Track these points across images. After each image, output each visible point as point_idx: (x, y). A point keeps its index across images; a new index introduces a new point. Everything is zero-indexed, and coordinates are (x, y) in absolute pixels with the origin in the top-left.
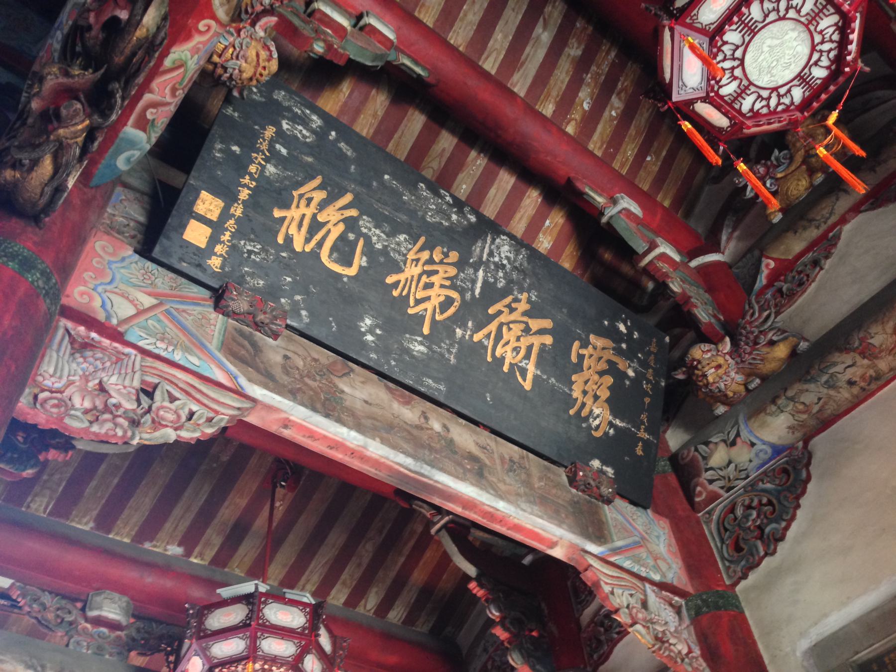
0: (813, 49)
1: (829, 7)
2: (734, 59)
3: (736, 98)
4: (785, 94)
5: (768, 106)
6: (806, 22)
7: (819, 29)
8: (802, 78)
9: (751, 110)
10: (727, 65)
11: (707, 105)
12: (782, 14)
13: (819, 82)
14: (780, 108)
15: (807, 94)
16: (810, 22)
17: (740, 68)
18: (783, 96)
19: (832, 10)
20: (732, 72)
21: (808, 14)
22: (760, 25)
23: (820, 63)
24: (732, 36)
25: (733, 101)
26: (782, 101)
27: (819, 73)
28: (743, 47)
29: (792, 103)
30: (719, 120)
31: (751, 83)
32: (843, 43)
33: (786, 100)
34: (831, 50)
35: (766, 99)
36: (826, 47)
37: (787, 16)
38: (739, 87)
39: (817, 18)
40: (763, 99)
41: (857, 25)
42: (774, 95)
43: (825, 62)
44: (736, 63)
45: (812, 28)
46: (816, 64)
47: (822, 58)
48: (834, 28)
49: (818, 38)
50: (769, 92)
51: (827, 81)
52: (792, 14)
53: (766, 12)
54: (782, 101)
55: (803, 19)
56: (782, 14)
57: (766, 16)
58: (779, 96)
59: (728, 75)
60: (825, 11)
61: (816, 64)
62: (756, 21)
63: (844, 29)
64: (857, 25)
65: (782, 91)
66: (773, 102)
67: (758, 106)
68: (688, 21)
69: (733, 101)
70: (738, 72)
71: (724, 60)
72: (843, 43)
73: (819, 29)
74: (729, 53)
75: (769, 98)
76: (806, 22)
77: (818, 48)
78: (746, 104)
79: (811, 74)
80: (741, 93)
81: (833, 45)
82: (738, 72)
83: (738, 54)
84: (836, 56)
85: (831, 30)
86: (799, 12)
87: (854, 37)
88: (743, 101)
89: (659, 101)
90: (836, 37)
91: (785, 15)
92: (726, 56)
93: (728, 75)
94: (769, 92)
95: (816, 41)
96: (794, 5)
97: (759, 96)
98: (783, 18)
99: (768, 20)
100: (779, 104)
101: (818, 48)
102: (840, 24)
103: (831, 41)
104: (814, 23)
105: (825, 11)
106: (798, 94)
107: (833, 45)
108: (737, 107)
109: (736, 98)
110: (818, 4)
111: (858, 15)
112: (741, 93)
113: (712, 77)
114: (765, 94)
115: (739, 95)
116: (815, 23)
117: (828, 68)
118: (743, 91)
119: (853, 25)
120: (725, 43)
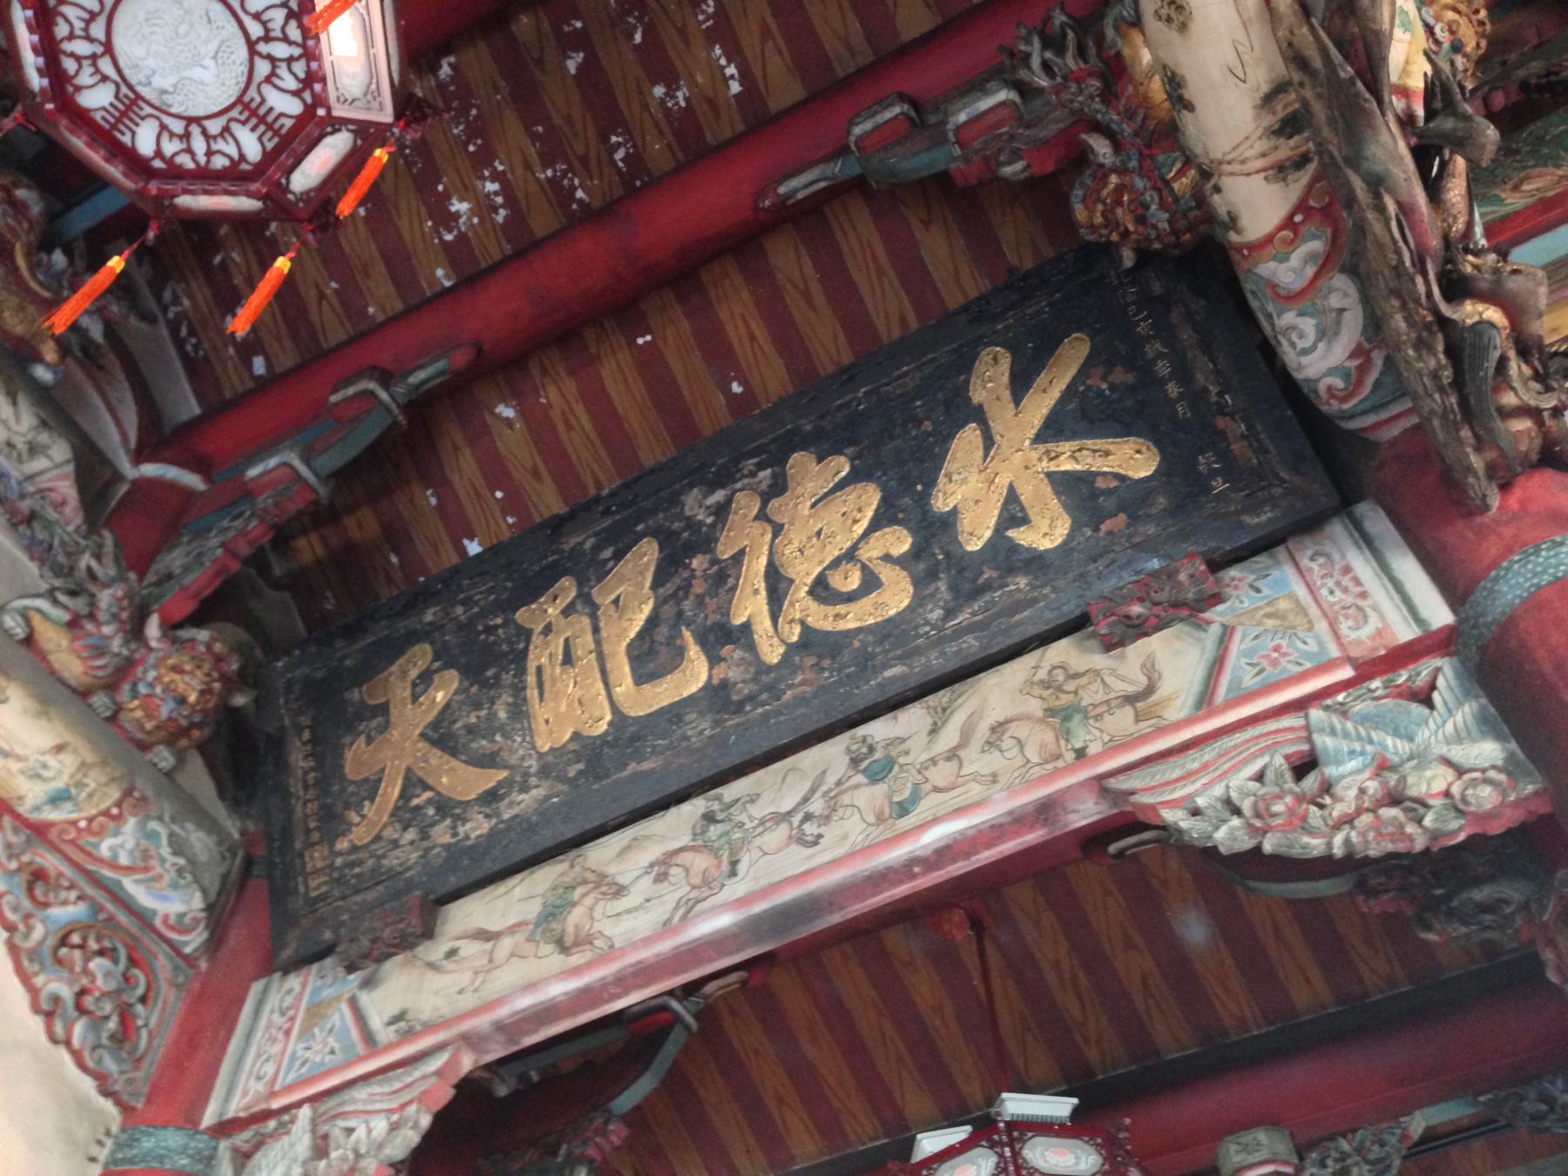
1: (276, 140)
6: (246, 99)
8: (131, 104)
9: (296, 94)
10: (199, 145)
12: (262, 48)
15: (98, 116)
16: (246, 106)
17: (206, 123)
18: (267, 30)
19: (270, 146)
20: (215, 137)
22: (124, 90)
23: (165, 137)
27: (145, 140)
28: (167, 120)
29: (78, 89)
31: (239, 100)
32: (205, 177)
33: (85, 78)
35: (274, 67)
38: (244, 123)
39: (254, 121)
40: (273, 74)
44: (195, 130)
45: (234, 113)
48: (236, 156)
50: (102, 37)
53: (265, 17)
54: (278, 34)
55: (252, 93)
56: (262, 48)
57: (105, 78)
58: (267, 38)
59: (220, 145)
60: (269, 134)
62: (117, 97)
63: (235, 176)
65: (256, 30)
67: (291, 84)
70: (214, 127)
71: (189, 151)
73: (235, 127)
75: (272, 59)
76: (246, 99)
79: (143, 118)
84: (180, 167)
90: (219, 162)
91: (260, 55)
93: (220, 145)
94: (257, 60)
97: (268, 80)
102: (244, 167)
103: (209, 153)
105: (269, 134)
106: (97, 98)
107: (202, 160)
109: (270, 127)
114: (263, 68)
116: (243, 118)
117: (159, 153)
120: (159, 153)
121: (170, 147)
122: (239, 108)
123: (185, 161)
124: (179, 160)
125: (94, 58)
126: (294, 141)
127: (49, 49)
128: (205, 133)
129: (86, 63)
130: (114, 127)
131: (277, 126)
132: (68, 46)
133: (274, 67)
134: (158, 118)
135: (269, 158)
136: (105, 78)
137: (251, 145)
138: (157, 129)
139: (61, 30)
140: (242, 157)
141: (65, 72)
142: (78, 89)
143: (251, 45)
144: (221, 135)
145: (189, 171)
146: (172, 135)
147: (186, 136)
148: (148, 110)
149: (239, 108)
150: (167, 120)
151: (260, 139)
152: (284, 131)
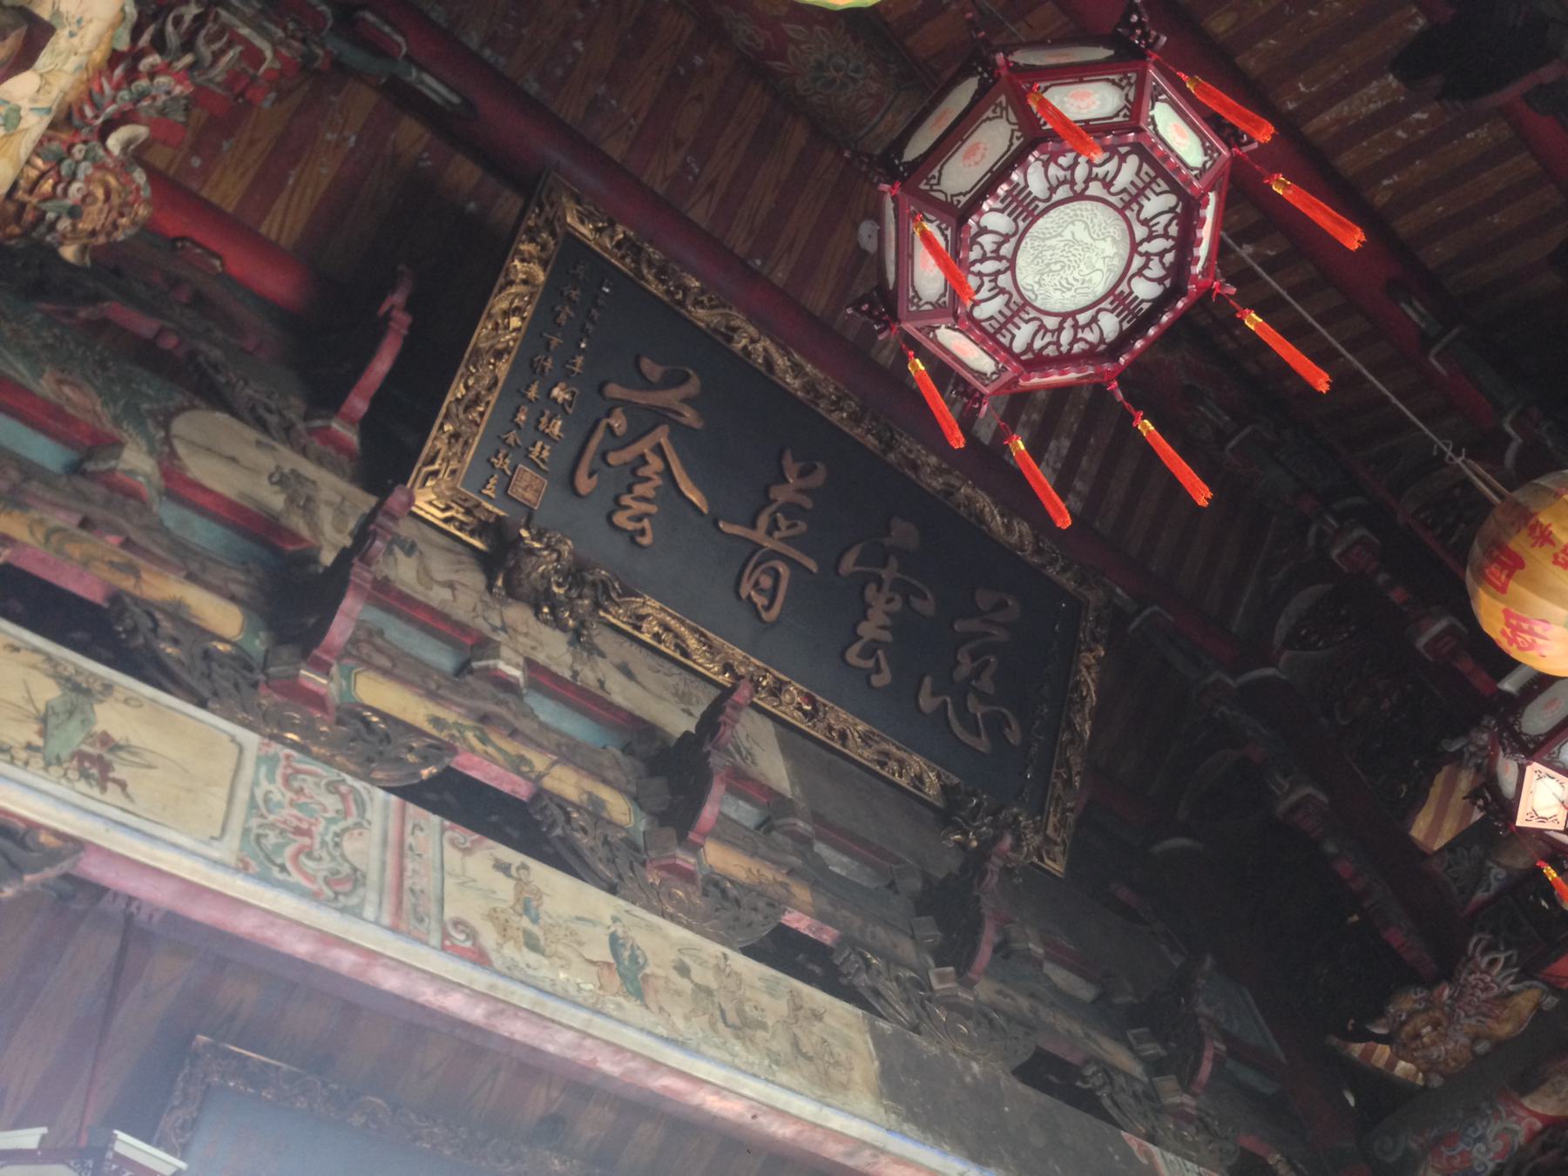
0: (1134, 247)
1: (1160, 181)
2: (999, 258)
3: (1003, 326)
4: (1088, 325)
5: (1058, 344)
6: (1120, 205)
7: (1142, 216)
8: (1117, 297)
9: (1123, 158)
10: (989, 267)
11: (957, 334)
12: (1078, 188)
13: (1145, 306)
14: (1077, 348)
15: (1126, 326)
16: (1127, 205)
18: (1083, 327)
19: (1164, 187)
20: (995, 280)
21: (1124, 190)
22: (1042, 206)
23: (1147, 272)
24: (994, 219)
25: (998, 331)
26: (1080, 335)
27: (1145, 290)
28: (1013, 240)
29: (1102, 340)
30: (977, 359)
31: (1121, 211)
33: (1092, 336)
34: (1166, 251)
35: (1096, 178)
36: (1157, 245)
37: (1088, 193)
38: (1007, 305)
41: (1209, 213)
42: (1069, 323)
43: (1155, 270)
45: (1016, 297)
46: (1139, 273)
47: (1151, 264)
48: (1169, 216)
49: (1140, 232)
51: (1160, 304)
52: (1051, 323)
53: (1054, 182)
54: (1080, 335)
55: (1033, 314)
56: (1069, 323)
57: (1052, 190)
58: (1076, 326)
59: (987, 285)
61: (1139, 273)
64: (1209, 213)
65: (1083, 318)
66: (1066, 337)
67: (1111, 167)
68: (923, 186)
69: (998, 331)
70: (1140, 232)
71: (1161, 254)
72: (1185, 243)
73: (1142, 216)
74: (989, 247)
75: (1060, 329)
76: (1120, 205)
77: (1004, 265)
78: (1021, 336)
80: (1134, 197)
81: (977, 268)
82: (1004, 281)
83: (1006, 250)
85: (1164, 219)
86: (1107, 185)
87: (1205, 233)
88: (1015, 331)
89: (878, 320)
92: (1161, 261)
93: (1159, 229)
95: (1138, 237)
96: (1101, 176)
97: (1042, 326)
98: (1064, 316)
99: (1056, 198)
100: (1075, 340)
101: (1143, 249)
103: (1166, 235)
104: (1135, 207)
105: (1154, 186)
106: (1110, 325)
107: (1170, 243)
108: (1005, 341)
110: (1142, 174)
111: (1212, 196)
112: (1134, 197)
113: (956, 289)
114: (1051, 323)
115: (1009, 320)
117: (1160, 281)
118: (1016, 314)
119: (1202, 212)
120: (1160, 281)
121: (987, 241)
122: (1020, 302)
123: (1169, 258)
124: (976, 248)
125: (1073, 183)
126: (1159, 164)
127: (1064, 360)
128: (998, 273)
129: (1068, 173)
130: (1135, 316)
131: (1147, 179)
132: (1064, 349)
133: (1096, 178)
134: (1133, 276)
135: (1174, 188)
136: (1052, 190)
137: (1157, 204)
138: (1003, 231)
139: (1051, 351)
140: (1172, 210)
141: (1084, 351)
142: (1102, 340)
143: (1073, 314)
144: (996, 287)
145: (1176, 256)
146: (1000, 245)
147: (1148, 255)
148: (1022, 225)
149: (1020, 302)
150: (1013, 240)
151: (992, 318)
152: (1153, 174)
